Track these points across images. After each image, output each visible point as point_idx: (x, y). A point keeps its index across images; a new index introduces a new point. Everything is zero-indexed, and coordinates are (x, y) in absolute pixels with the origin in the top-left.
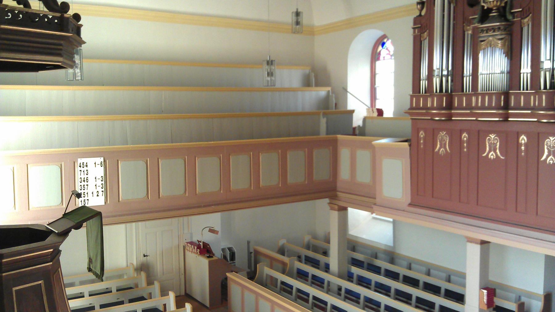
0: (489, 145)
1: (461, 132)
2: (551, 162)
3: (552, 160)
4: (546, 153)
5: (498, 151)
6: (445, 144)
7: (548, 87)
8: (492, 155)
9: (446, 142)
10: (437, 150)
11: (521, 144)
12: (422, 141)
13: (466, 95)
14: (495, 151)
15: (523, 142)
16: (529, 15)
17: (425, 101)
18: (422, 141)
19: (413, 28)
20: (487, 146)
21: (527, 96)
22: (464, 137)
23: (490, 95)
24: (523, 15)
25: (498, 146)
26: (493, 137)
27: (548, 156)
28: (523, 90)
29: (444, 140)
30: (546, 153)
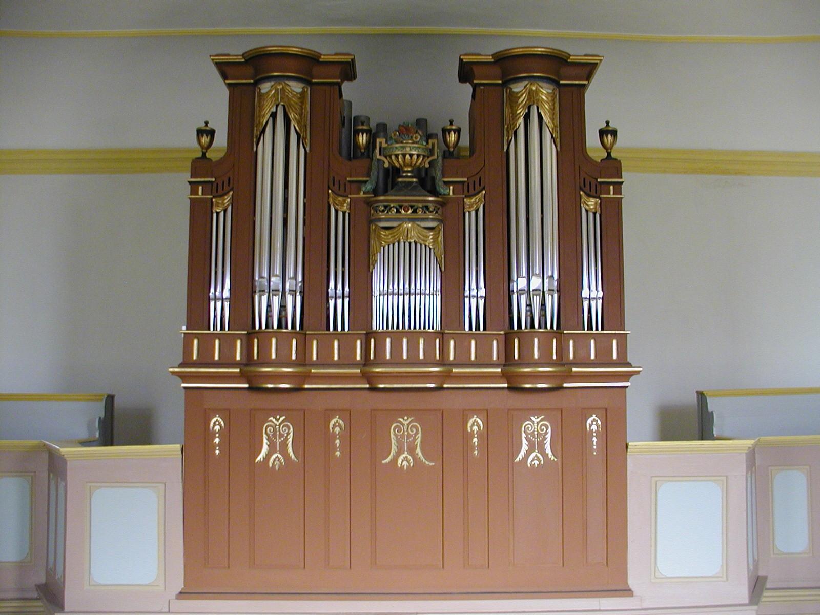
0: (398, 441)
1: (328, 415)
2: (536, 462)
3: (538, 459)
4: (525, 447)
5: (418, 450)
6: (284, 444)
7: (536, 326)
8: (406, 459)
9: (286, 439)
10: (260, 457)
11: (472, 435)
12: (217, 440)
13: (341, 336)
14: (412, 451)
15: (594, 428)
16: (228, 192)
17: (304, 349)
18: (217, 440)
19: (190, 182)
20: (393, 441)
21: (227, 342)
22: (334, 426)
23: (413, 336)
24: (469, 189)
25: (419, 441)
26: (406, 423)
27: (528, 453)
28: (597, 329)
29: (281, 436)
30: (525, 447)
